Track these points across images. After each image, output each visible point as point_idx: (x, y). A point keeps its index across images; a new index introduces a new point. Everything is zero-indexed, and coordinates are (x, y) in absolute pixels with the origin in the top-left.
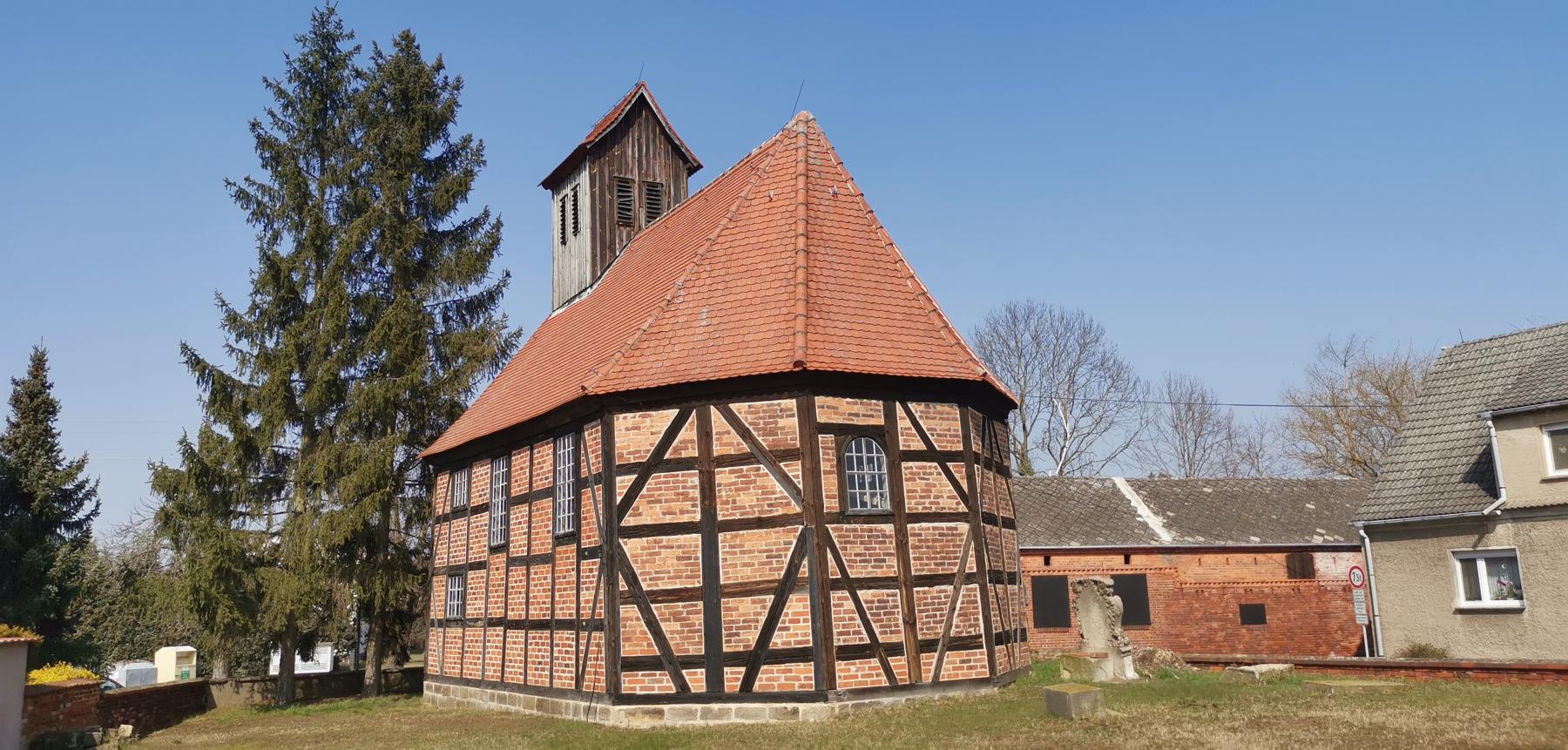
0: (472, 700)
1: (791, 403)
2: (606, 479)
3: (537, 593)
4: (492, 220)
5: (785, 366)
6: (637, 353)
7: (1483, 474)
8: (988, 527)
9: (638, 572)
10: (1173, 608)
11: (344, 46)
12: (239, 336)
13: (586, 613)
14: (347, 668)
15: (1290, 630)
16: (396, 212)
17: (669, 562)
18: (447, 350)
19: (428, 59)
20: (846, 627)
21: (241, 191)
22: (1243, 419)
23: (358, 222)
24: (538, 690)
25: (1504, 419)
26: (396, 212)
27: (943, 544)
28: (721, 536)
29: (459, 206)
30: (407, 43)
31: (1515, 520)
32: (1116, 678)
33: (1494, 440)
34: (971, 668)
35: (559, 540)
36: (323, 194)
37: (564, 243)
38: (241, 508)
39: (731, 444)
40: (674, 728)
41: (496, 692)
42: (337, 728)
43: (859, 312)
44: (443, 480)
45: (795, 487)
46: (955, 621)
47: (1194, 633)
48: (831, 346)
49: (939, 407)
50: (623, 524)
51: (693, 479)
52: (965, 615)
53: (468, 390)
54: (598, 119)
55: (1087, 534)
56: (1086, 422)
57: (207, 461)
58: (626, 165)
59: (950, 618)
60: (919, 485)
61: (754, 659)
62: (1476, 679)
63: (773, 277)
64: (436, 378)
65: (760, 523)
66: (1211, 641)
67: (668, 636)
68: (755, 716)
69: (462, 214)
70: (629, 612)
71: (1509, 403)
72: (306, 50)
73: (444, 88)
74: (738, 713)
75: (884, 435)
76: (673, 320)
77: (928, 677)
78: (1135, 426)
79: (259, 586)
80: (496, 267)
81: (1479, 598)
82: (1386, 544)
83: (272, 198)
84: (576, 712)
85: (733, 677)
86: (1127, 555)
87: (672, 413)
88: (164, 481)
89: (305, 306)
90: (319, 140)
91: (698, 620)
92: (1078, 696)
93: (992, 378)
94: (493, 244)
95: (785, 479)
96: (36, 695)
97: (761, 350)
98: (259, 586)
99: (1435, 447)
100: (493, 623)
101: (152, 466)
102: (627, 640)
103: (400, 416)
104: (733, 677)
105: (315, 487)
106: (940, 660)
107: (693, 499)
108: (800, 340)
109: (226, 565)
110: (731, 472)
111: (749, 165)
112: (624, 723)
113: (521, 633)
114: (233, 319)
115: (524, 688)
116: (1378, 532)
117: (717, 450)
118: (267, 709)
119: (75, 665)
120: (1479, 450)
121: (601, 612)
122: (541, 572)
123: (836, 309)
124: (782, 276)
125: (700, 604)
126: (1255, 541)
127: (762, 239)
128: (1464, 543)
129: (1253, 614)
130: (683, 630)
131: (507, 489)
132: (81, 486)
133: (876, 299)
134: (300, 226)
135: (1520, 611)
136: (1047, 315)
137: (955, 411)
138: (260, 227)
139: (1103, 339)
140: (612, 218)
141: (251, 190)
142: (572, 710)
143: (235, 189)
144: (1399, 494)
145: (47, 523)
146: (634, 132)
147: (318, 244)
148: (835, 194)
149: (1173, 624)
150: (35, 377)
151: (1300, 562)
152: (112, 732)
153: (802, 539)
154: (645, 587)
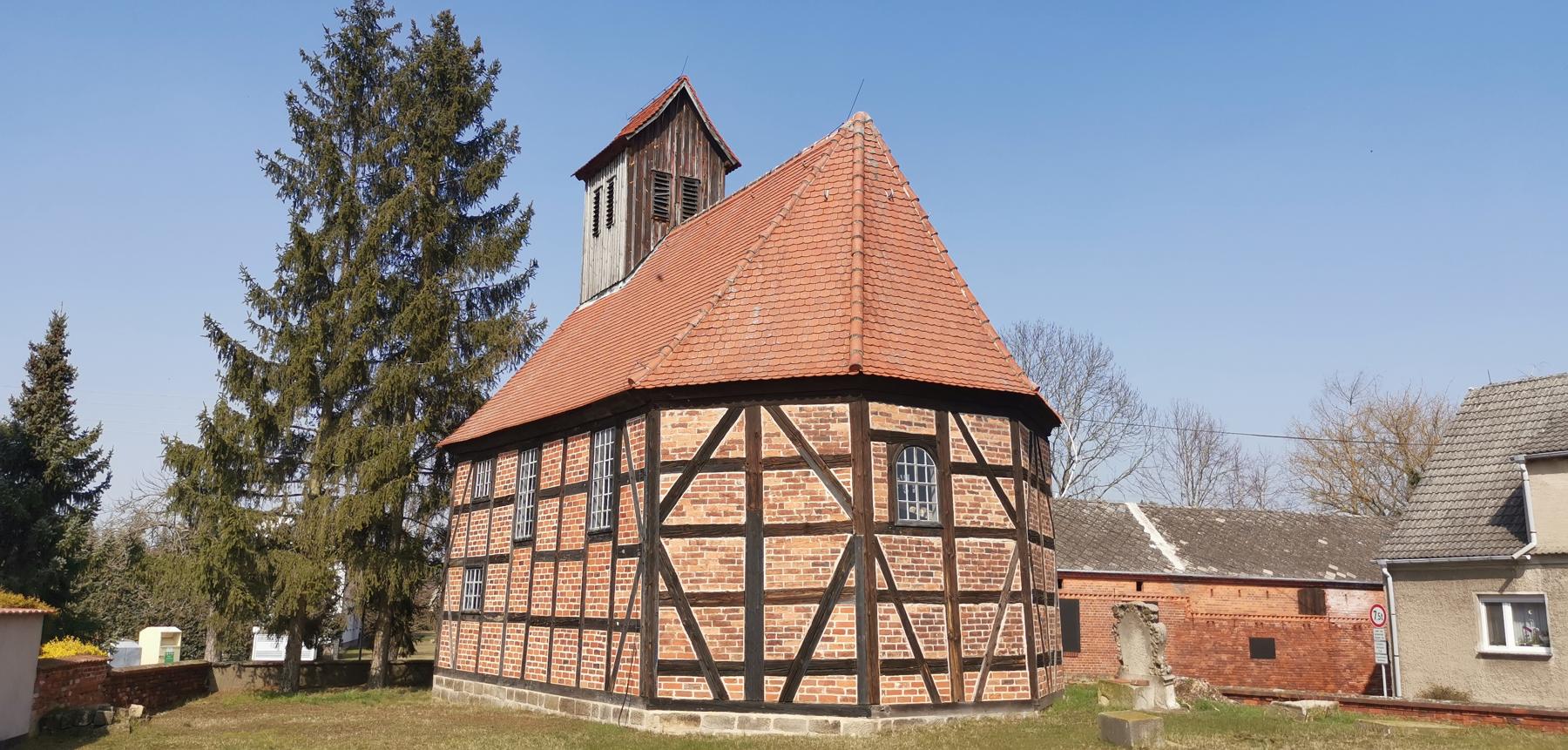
0: (488, 696)
1: (845, 408)
2: (650, 475)
3: (565, 591)
4: (523, 207)
5: (841, 369)
6: (687, 348)
7: (1513, 517)
8: (1034, 545)
9: (679, 573)
10: (1183, 638)
11: (384, 23)
12: (262, 313)
13: (620, 613)
14: (331, 657)
15: (1299, 666)
16: (428, 195)
17: (711, 564)
18: (470, 339)
19: (467, 42)
20: (892, 642)
21: (273, 164)
22: (1251, 450)
23: (391, 202)
24: (562, 690)
25: (1537, 463)
26: (428, 195)
27: (989, 561)
28: (766, 540)
29: (488, 192)
30: (446, 24)
31: (1545, 566)
32: (1156, 707)
33: (1527, 484)
34: (1013, 689)
35: (592, 537)
36: (355, 173)
37: (596, 235)
38: (255, 488)
39: (780, 447)
40: (710, 737)
41: (515, 690)
42: (352, 719)
43: (915, 318)
44: (464, 470)
45: (845, 494)
46: (999, 640)
47: (1203, 665)
48: (887, 351)
49: (991, 420)
50: (665, 523)
51: (739, 480)
52: (1009, 634)
53: (490, 380)
54: (635, 112)
55: (1100, 558)
56: (1090, 446)
57: (224, 437)
58: (664, 158)
59: (994, 637)
60: (968, 498)
61: (796, 669)
62: (1527, 727)
63: (828, 278)
64: (458, 366)
65: (808, 529)
66: (1219, 674)
67: (707, 640)
68: (794, 728)
69: (492, 200)
70: (669, 614)
71: (1541, 448)
72: (346, 25)
73: (480, 72)
74: (777, 724)
75: (934, 445)
76: (723, 317)
77: (970, 697)
78: (1140, 452)
79: (271, 568)
80: (523, 257)
81: (1504, 643)
82: (1409, 583)
83: (302, 174)
84: (605, 714)
85: (773, 686)
86: (1140, 581)
87: (721, 412)
88: (179, 457)
89: (331, 284)
90: (355, 118)
91: (739, 626)
92: (1137, 724)
93: (1042, 394)
94: (522, 232)
95: (835, 485)
96: (49, 670)
97: (815, 352)
98: (271, 568)
99: (1462, 488)
100: (514, 618)
101: (165, 440)
102: (666, 642)
103: (419, 402)
104: (773, 686)
105: (332, 471)
106: (983, 680)
107: (739, 501)
108: (856, 344)
109: (242, 545)
110: (779, 476)
111: (802, 164)
112: (716, 731)
113: (546, 630)
114: (257, 295)
115: (547, 687)
116: (1402, 571)
117: (766, 452)
118: (273, 695)
119: (84, 641)
120: (1508, 493)
121: (638, 613)
122: (570, 569)
123: (891, 315)
124: (837, 277)
125: (742, 610)
126: (1268, 574)
127: (819, 238)
128: (1491, 587)
129: (1262, 648)
130: (724, 636)
131: (535, 483)
132: (93, 457)
133: (931, 307)
134: (330, 204)
135: (1546, 658)
136: (1056, 337)
137: (1005, 425)
138: (290, 202)
139: (1111, 364)
140: (648, 212)
141: (282, 164)
142: (601, 712)
143: (267, 162)
144: (1423, 534)
145: (59, 492)
146: (674, 127)
147: (347, 223)
148: (891, 197)
149: (1182, 655)
150: (53, 343)
151: (1312, 598)
152: (122, 711)
153: (850, 549)
154: (685, 590)
